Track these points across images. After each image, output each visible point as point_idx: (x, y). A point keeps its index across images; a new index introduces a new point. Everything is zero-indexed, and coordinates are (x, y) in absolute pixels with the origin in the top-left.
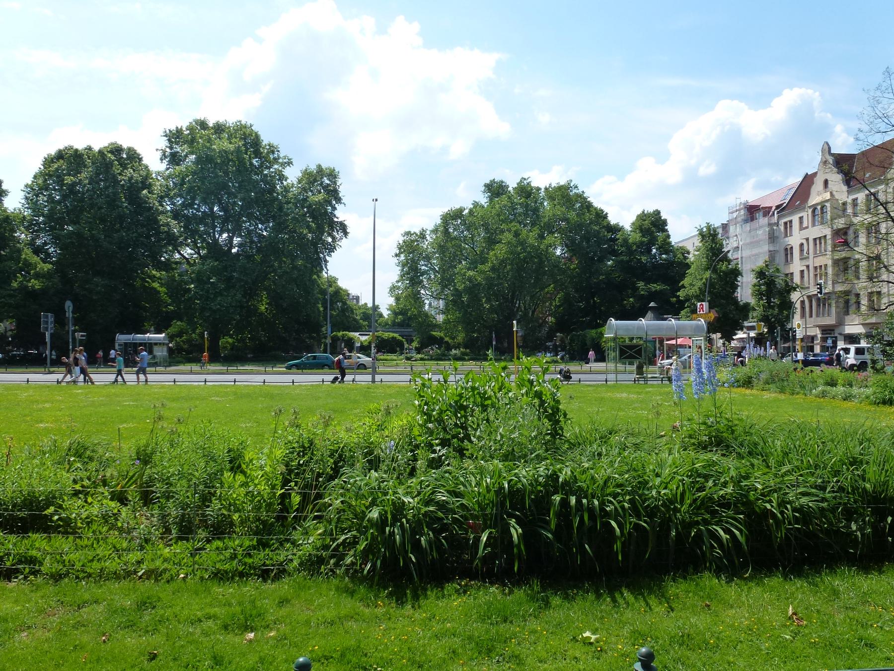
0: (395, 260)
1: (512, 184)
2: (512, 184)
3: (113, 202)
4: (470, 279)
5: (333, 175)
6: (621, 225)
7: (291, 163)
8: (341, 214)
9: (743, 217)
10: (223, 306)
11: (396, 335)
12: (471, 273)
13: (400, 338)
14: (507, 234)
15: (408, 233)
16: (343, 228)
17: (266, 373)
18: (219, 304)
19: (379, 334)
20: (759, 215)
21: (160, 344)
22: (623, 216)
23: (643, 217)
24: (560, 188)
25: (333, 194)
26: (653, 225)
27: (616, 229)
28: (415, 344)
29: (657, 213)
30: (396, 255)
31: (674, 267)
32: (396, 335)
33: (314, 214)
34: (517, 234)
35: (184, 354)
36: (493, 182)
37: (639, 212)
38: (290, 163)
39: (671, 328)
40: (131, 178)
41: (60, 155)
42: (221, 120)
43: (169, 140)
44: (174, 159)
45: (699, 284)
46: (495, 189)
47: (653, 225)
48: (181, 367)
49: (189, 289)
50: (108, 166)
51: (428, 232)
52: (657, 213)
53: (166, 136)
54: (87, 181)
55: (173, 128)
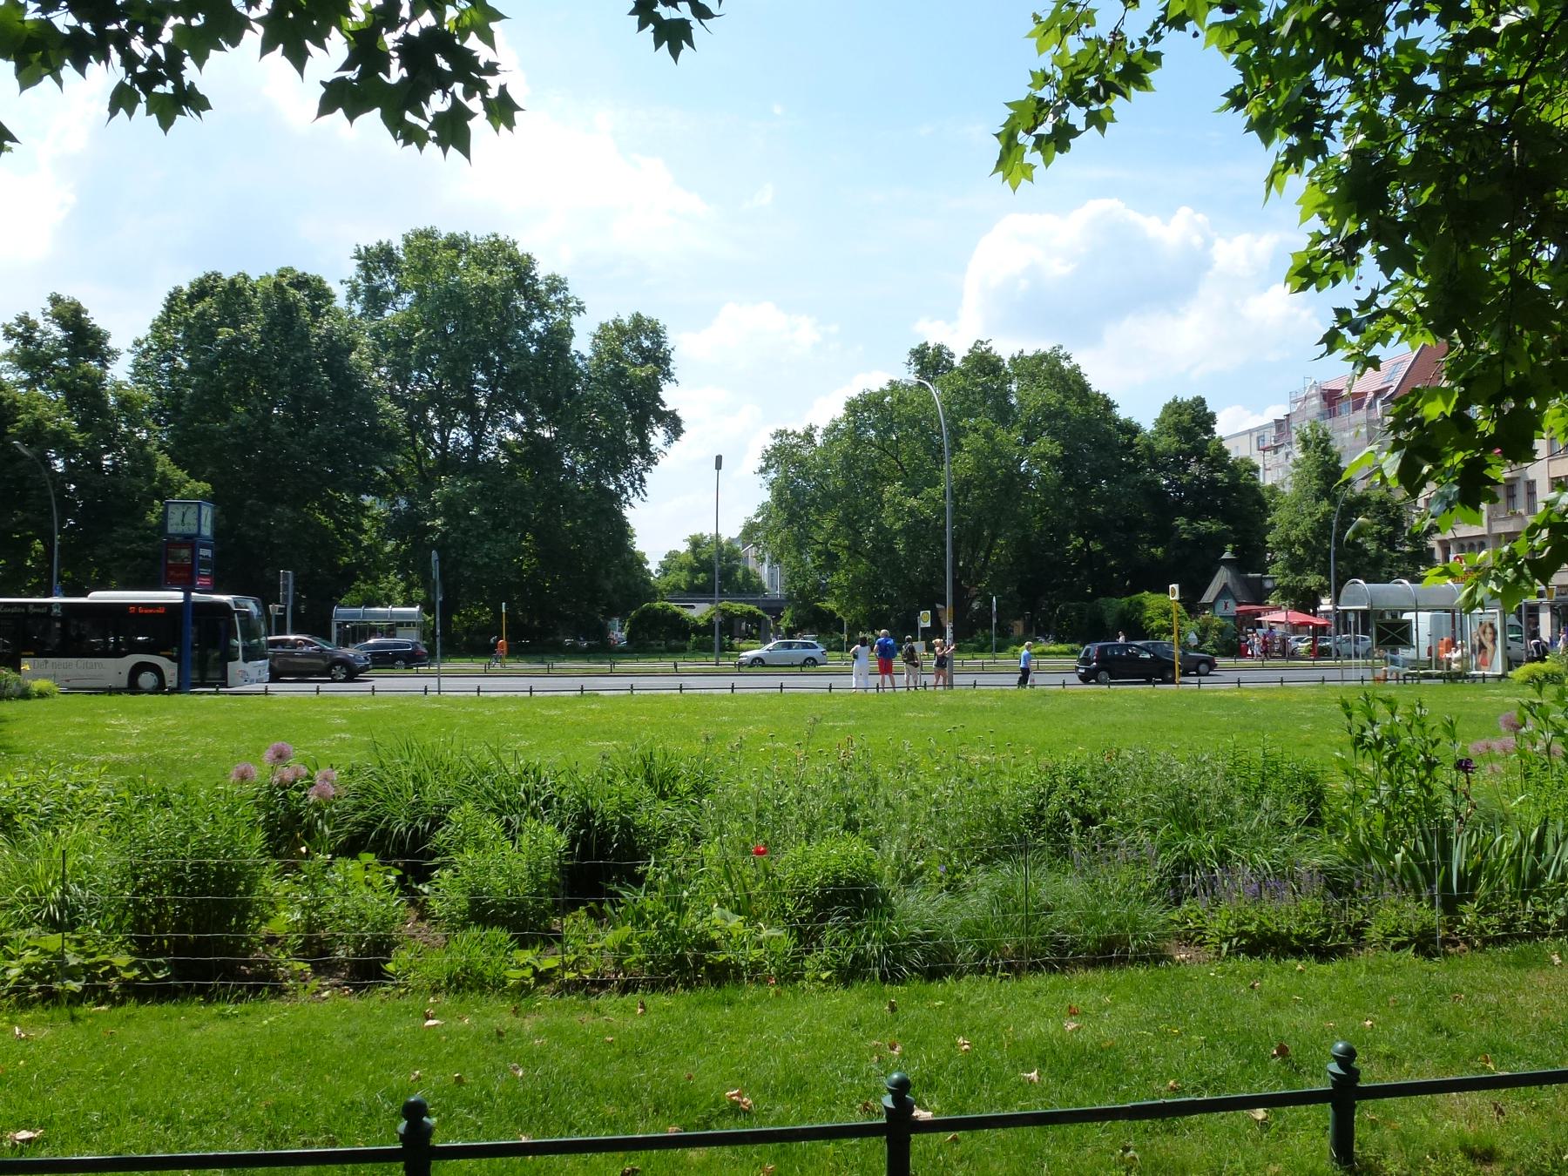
0: (759, 478)
1: (959, 350)
2: (959, 350)
3: (302, 373)
4: (911, 512)
5: (656, 332)
6: (1135, 420)
7: (583, 309)
8: (671, 397)
9: (1318, 410)
10: (493, 559)
11: (753, 608)
12: (912, 502)
13: (760, 612)
14: (972, 436)
15: (781, 434)
16: (674, 426)
17: (983, 671)
18: (487, 555)
19: (725, 605)
20: (1342, 406)
21: (408, 624)
22: (1141, 408)
23: (1175, 408)
24: (1042, 358)
25: (658, 359)
26: (1192, 421)
27: (1131, 429)
28: (785, 624)
29: (1200, 402)
30: (762, 470)
31: (1233, 498)
32: (753, 608)
33: (624, 399)
34: (988, 436)
35: (457, 640)
36: (925, 346)
37: (1169, 400)
38: (580, 309)
39: (1407, 594)
40: (331, 332)
41: (202, 290)
42: (459, 232)
43: (364, 266)
44: (376, 300)
45: (1307, 522)
46: (930, 361)
47: (1192, 421)
48: (447, 666)
49: (433, 529)
50: (289, 309)
51: (820, 432)
52: (1200, 402)
53: (359, 258)
54: (256, 337)
55: (373, 244)
